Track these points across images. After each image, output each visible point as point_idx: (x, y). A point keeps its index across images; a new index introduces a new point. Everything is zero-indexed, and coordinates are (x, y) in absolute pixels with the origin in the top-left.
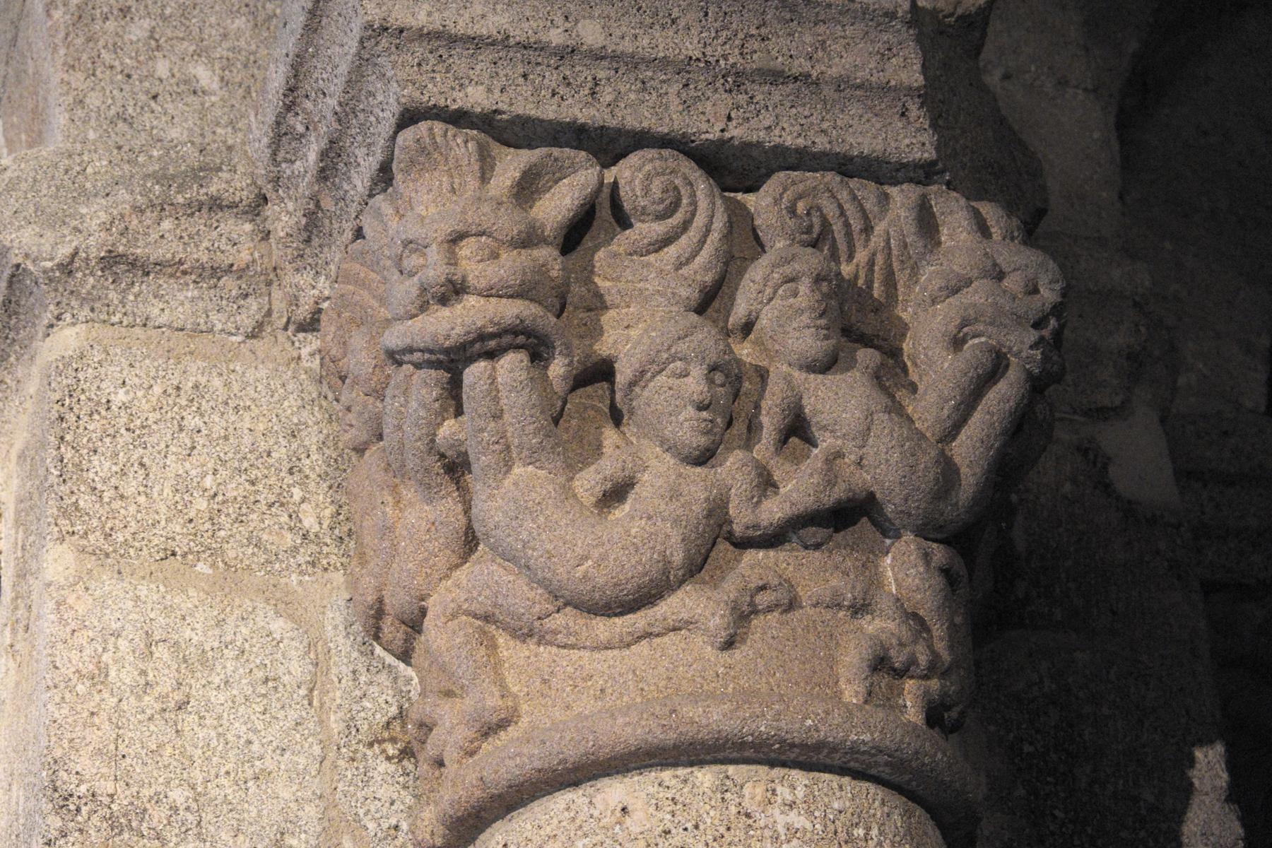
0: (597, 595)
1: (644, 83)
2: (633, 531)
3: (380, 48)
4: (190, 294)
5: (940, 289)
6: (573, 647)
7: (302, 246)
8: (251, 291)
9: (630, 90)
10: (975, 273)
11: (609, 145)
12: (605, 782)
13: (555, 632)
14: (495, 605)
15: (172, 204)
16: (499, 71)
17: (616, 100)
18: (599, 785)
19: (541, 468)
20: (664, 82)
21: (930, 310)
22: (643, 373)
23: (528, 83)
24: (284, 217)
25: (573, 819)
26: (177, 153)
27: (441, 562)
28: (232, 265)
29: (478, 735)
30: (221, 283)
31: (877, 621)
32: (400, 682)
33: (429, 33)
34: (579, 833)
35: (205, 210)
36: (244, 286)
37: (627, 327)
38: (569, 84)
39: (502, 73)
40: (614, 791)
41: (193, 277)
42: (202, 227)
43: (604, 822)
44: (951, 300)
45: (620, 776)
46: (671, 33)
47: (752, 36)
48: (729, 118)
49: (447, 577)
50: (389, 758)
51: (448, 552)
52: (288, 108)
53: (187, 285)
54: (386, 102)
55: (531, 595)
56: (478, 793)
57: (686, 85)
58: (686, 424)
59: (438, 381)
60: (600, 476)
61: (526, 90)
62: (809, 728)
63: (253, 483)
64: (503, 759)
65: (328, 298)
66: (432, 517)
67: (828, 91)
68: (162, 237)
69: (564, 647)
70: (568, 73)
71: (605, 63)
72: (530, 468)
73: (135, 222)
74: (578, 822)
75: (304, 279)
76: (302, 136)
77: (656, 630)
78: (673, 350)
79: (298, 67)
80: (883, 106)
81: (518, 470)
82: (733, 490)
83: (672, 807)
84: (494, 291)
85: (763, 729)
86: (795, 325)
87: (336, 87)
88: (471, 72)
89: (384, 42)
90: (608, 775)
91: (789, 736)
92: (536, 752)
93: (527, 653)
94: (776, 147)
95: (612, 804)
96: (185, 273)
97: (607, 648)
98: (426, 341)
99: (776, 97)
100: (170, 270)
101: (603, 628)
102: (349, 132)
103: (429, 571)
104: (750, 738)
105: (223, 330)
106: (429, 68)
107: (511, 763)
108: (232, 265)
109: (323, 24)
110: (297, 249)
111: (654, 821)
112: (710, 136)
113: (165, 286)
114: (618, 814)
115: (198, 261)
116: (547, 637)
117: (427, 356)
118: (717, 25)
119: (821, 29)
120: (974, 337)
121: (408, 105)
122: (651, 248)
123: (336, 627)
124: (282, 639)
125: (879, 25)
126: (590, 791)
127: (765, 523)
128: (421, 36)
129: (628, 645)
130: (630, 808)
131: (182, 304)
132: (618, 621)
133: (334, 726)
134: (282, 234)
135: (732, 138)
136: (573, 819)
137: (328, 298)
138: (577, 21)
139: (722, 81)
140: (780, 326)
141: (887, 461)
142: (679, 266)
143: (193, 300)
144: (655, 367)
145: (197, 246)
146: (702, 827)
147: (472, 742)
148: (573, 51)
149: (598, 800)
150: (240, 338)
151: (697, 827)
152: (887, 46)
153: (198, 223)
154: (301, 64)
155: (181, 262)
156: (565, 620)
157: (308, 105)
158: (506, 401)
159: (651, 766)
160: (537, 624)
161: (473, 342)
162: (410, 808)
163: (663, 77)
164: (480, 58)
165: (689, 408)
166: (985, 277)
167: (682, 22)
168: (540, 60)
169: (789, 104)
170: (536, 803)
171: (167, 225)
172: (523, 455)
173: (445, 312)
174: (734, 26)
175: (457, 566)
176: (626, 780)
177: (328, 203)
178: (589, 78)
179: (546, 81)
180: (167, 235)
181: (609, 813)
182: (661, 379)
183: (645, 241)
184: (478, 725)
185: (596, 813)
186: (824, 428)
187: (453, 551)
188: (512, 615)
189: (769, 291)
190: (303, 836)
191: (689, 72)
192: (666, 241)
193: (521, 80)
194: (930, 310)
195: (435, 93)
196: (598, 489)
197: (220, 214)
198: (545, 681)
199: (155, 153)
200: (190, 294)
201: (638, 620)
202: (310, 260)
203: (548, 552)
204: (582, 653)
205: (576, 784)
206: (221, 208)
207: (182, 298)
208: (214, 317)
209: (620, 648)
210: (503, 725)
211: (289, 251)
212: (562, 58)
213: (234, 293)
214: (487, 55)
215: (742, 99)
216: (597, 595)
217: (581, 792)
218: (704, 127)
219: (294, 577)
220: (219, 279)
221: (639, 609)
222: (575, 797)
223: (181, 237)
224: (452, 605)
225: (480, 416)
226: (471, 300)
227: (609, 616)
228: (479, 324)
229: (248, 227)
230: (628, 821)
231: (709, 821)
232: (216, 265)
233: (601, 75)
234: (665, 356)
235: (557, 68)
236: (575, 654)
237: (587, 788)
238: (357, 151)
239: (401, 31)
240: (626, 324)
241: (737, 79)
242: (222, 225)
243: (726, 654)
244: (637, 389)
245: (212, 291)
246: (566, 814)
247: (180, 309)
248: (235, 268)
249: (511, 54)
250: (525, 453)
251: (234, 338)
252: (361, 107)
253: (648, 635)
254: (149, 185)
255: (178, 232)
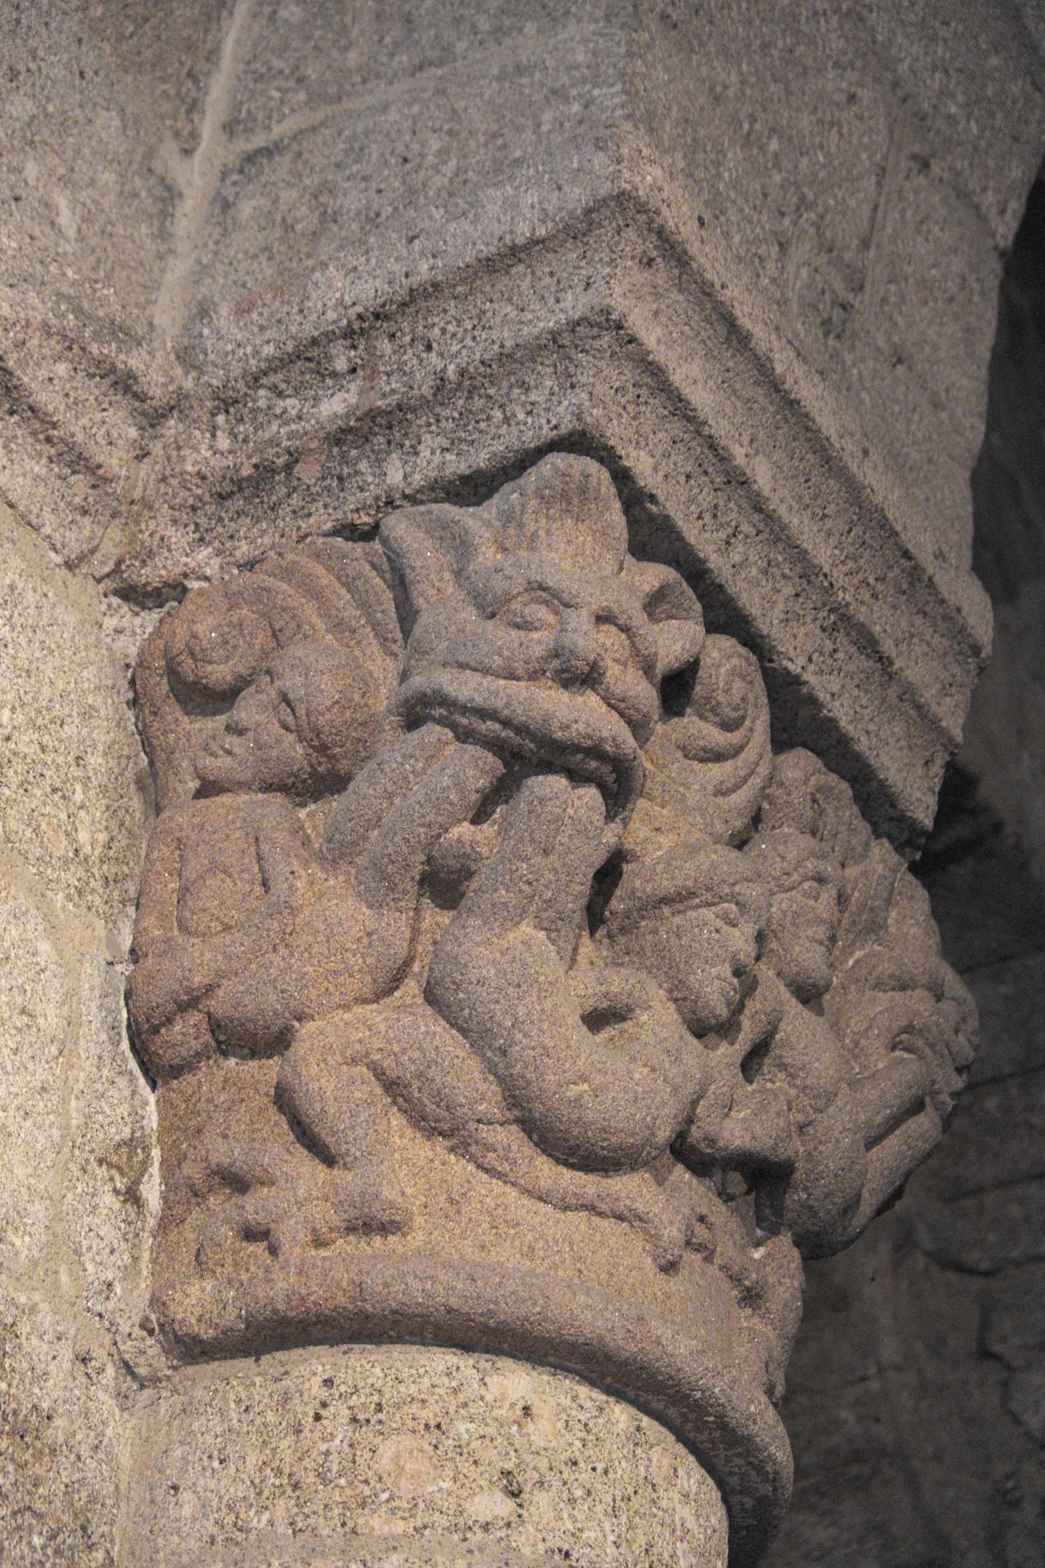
0: (576, 1131)
1: (769, 564)
2: (637, 1076)
3: (596, 344)
4: (37, 469)
5: (892, 976)
6: (499, 1175)
7: (207, 498)
8: (93, 510)
9: (756, 563)
10: (924, 979)
11: (724, 617)
12: (506, 1363)
13: (490, 1148)
14: (420, 1075)
15: (83, 349)
16: (673, 453)
17: (741, 565)
18: (499, 1364)
19: (554, 942)
20: (784, 576)
21: (868, 993)
22: (692, 894)
23: (687, 487)
24: (209, 451)
25: (455, 1391)
26: (95, 291)
27: (354, 985)
28: (100, 466)
29: (344, 1225)
30: (72, 479)
31: (756, 1320)
32: (137, 1102)
33: (651, 363)
34: (462, 1412)
35: (107, 381)
36: (91, 499)
37: (657, 830)
38: (715, 516)
39: (673, 458)
40: (516, 1382)
41: (53, 451)
42: (92, 398)
43: (497, 1413)
44: (894, 993)
45: (529, 1366)
46: (815, 528)
47: (868, 584)
48: (810, 660)
49: (347, 1007)
50: (116, 1191)
51: (369, 978)
52: (349, 333)
53: (41, 456)
54: (544, 408)
55: (482, 1087)
56: (341, 1300)
57: (797, 595)
58: (717, 983)
59: (492, 769)
60: (603, 989)
61: (683, 494)
62: (751, 1414)
63: (43, 748)
64: (404, 1275)
65: (207, 579)
66: (371, 925)
67: (892, 692)
68: (51, 380)
69: (487, 1171)
70: (721, 503)
71: (756, 517)
72: (542, 935)
73: (35, 342)
74: (462, 1398)
75: (179, 538)
76: (334, 374)
77: (604, 1207)
78: (737, 889)
79: (418, 298)
80: (919, 742)
81: (526, 928)
82: (713, 1087)
83: (583, 1434)
84: (623, 705)
85: (717, 1390)
86: (810, 933)
87: (474, 352)
88: (651, 436)
89: (605, 341)
90: (514, 1357)
91: (731, 1414)
92: (460, 1286)
93: (430, 1154)
94: (831, 720)
95: (514, 1396)
96: (49, 440)
97: (540, 1199)
98: (520, 714)
99: (851, 667)
100: (37, 425)
101: (546, 1172)
102: (438, 410)
103: (331, 988)
104: (698, 1395)
105: (49, 537)
106: (623, 400)
107: (416, 1285)
108: (100, 466)
109: (514, 271)
110: (200, 498)
111: (562, 1442)
112: (791, 667)
113: (20, 441)
114: (519, 1412)
115: (73, 435)
116: (473, 1149)
117: (507, 734)
118: (851, 549)
119: (918, 620)
120: (905, 1049)
121: (588, 429)
122: (701, 754)
123: (92, 989)
124: (46, 968)
125: (960, 653)
126: (483, 1365)
127: (721, 1143)
128: (643, 360)
129: (566, 1209)
130: (534, 1411)
131: (24, 475)
132: (568, 1174)
133: (75, 1114)
134: (190, 469)
135: (806, 682)
136: (455, 1391)
137: (207, 579)
138: (757, 452)
139: (826, 614)
140: (793, 924)
141: (838, 1141)
142: (719, 793)
143: (37, 478)
144: (708, 897)
145: (77, 418)
146: (611, 1475)
147: (331, 1229)
148: (743, 483)
149: (493, 1380)
150: (58, 559)
151: (606, 1472)
152: (951, 680)
153: (91, 390)
154: (427, 296)
155: (54, 425)
156: (508, 1138)
157: (385, 346)
158: (565, 840)
159: (570, 1371)
160: (472, 1126)
161: (576, 748)
162: (126, 1267)
163: (787, 571)
164: (667, 426)
165: (727, 965)
166: (929, 989)
167: (829, 524)
168: (710, 470)
169: (856, 681)
170: (399, 1347)
171: (62, 369)
172: (544, 915)
173: (565, 696)
174: (862, 561)
175: (365, 1001)
176: (535, 1373)
177: (307, 472)
178: (733, 524)
179: (700, 497)
180: (56, 381)
181: (507, 1405)
182: (709, 914)
183: (701, 743)
184: (353, 1213)
185: (489, 1398)
186: (783, 1066)
187: (375, 981)
188: (438, 1098)
189: (795, 877)
190: (27, 1238)
191: (809, 582)
192: (717, 756)
193: (682, 479)
194: (868, 993)
195: (616, 433)
196: (591, 1002)
197: (119, 397)
198: (451, 1200)
199: (70, 273)
200: (37, 469)
201: (571, 1180)
202: (203, 521)
203: (544, 1048)
204: (508, 1189)
205: (466, 1347)
206: (127, 389)
207: (28, 468)
208: (47, 515)
209: (555, 1206)
210: (386, 1229)
211: (183, 493)
212: (729, 482)
213: (77, 500)
214: (676, 428)
215: (829, 646)
216: (576, 1131)
217: (471, 1362)
218: (792, 653)
219: (61, 896)
220: (74, 472)
221: (591, 1171)
222: (462, 1364)
223: (67, 395)
224: (358, 1047)
225: (532, 841)
226: (592, 700)
227: (558, 1161)
228: (605, 734)
229: (133, 433)
230: (530, 1427)
231: (620, 1472)
232: (86, 454)
233: (745, 528)
234: (727, 890)
235: (715, 490)
236: (497, 1185)
237: (484, 1361)
238: (427, 437)
239: (630, 342)
240: (657, 825)
241: (842, 622)
242: (111, 411)
243: (662, 1276)
244: (666, 911)
245: (59, 482)
246: (446, 1380)
247: (20, 479)
248: (101, 472)
249: (694, 444)
250: (551, 913)
251: (53, 555)
252: (491, 392)
253: (591, 1208)
254: (63, 307)
255: (68, 386)
